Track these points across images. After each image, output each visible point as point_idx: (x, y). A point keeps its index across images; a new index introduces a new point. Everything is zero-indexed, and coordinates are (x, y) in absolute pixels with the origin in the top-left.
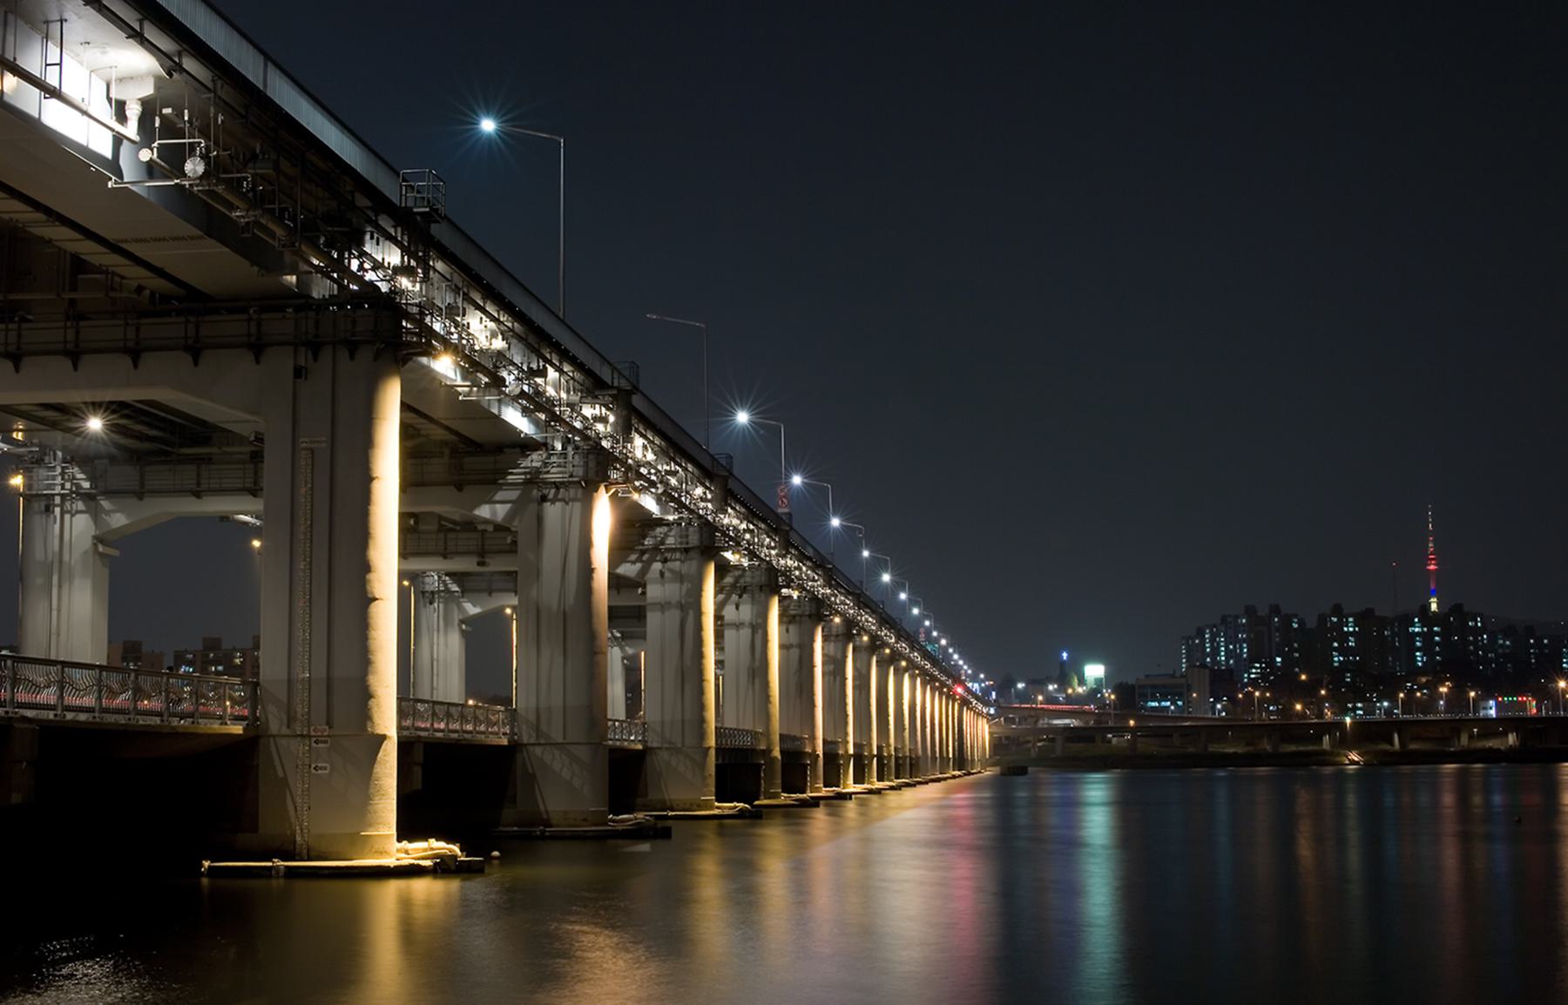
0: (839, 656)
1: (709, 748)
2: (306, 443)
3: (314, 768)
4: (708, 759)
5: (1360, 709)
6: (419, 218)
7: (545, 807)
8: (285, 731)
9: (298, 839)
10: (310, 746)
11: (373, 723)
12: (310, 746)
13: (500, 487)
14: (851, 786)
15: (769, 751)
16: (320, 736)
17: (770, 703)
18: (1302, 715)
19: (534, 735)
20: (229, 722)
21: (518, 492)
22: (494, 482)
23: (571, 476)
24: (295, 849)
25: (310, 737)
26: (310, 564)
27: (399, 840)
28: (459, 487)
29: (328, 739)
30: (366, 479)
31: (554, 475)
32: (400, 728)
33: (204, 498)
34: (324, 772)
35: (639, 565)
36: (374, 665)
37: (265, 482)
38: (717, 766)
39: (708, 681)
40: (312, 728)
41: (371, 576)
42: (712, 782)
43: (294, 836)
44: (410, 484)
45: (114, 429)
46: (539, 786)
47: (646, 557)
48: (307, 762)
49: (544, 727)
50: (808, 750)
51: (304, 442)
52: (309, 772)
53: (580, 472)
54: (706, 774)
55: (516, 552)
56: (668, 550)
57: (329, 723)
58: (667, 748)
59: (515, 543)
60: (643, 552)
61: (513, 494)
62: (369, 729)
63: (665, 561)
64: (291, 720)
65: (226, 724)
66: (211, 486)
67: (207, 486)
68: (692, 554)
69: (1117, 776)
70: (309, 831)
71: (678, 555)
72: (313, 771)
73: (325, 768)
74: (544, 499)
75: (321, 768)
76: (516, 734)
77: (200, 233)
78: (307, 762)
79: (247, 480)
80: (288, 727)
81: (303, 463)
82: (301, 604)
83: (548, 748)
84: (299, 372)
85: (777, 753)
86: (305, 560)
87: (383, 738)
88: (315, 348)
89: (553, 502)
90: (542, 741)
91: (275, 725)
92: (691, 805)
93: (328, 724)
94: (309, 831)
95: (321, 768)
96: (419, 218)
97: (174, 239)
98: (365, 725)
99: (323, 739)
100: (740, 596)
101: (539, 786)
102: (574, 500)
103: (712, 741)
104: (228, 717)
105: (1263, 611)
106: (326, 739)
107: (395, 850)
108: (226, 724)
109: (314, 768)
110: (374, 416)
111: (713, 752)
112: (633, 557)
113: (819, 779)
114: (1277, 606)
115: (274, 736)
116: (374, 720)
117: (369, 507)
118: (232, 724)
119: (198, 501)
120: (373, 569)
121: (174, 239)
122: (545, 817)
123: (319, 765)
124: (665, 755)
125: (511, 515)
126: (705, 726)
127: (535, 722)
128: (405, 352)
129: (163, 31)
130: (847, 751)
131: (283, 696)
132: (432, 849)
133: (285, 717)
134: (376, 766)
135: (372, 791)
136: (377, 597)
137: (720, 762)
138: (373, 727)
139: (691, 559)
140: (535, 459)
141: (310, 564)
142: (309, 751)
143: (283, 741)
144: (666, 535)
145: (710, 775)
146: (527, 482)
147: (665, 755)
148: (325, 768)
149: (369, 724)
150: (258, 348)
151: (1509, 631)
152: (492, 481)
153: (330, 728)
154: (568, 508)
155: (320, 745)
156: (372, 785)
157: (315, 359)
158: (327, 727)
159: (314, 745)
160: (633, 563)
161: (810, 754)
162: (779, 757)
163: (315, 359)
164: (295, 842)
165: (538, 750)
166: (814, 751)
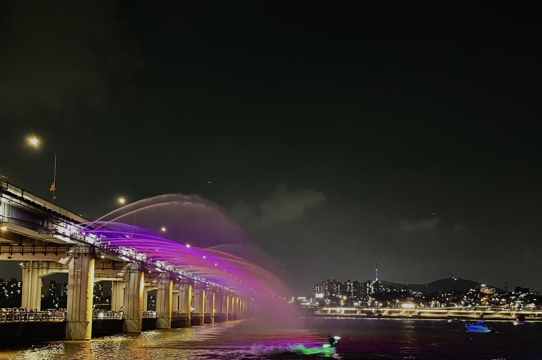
0: (212, 295)
1: (170, 318)
5: (444, 295)
13: (122, 270)
21: (126, 271)
22: (121, 269)
23: (136, 268)
28: (114, 269)
31: (133, 268)
35: (157, 281)
45: (26, 218)
47: (158, 279)
53: (138, 267)
56: (163, 278)
60: (158, 278)
61: (125, 271)
63: (162, 280)
68: (168, 279)
71: (165, 279)
74: (131, 272)
85: (190, 318)
89: (132, 273)
90: (129, 319)
100: (183, 285)
102: (137, 273)
105: (331, 281)
112: (156, 279)
114: (335, 280)
124: (160, 319)
125: (124, 275)
129: (67, 262)
130: (212, 315)
137: (172, 320)
139: (168, 280)
140: (129, 264)
144: (163, 275)
146: (127, 269)
147: (160, 319)
151: (390, 287)
152: (121, 268)
154: (135, 274)
160: (155, 280)
162: (190, 318)
165: (128, 320)
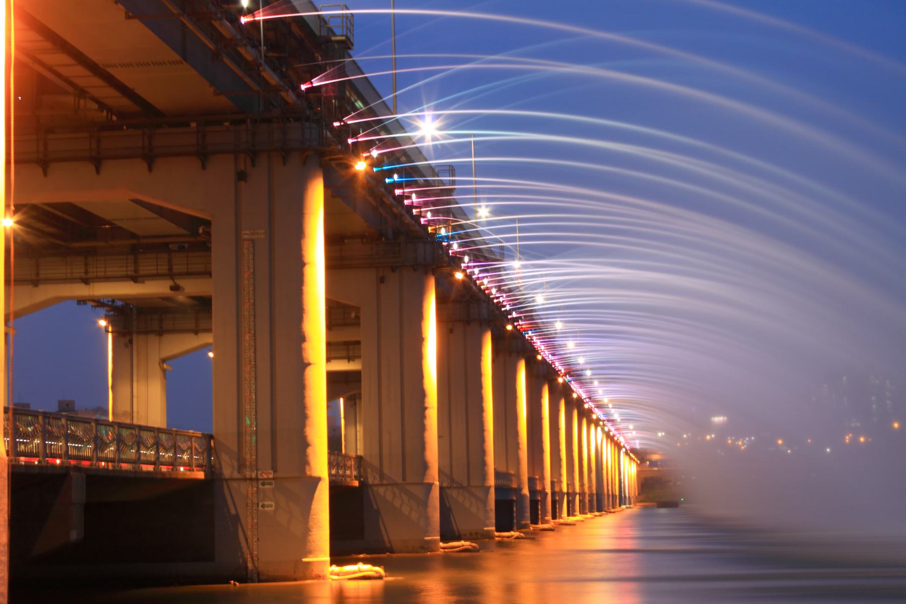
2: (248, 235)
3: (262, 506)
4: (489, 496)
6: (336, 46)
7: (388, 537)
8: (236, 475)
9: (250, 565)
10: (258, 488)
11: (311, 467)
12: (258, 488)
14: (565, 517)
15: (519, 489)
16: (266, 479)
17: (520, 449)
18: (183, 474)
19: (377, 477)
20: (195, 469)
24: (247, 574)
25: (257, 479)
26: (255, 335)
27: (332, 563)
29: (273, 482)
30: (299, 264)
32: (330, 475)
33: (91, 284)
34: (269, 509)
36: (310, 419)
37: (215, 267)
38: (497, 502)
39: (489, 431)
40: (259, 472)
41: (306, 345)
42: (492, 515)
43: (245, 562)
44: (333, 265)
46: (382, 520)
48: (255, 501)
49: (386, 471)
50: (514, 485)
51: (246, 234)
52: (257, 510)
54: (488, 508)
55: (359, 324)
57: (274, 469)
58: (455, 488)
59: (357, 318)
62: (308, 472)
64: (241, 466)
65: (193, 470)
66: (159, 272)
67: (95, 274)
69: (639, 507)
70: (258, 559)
72: (260, 508)
73: (271, 506)
75: (268, 506)
76: (362, 477)
77: (178, 57)
78: (255, 501)
79: (129, 269)
80: (239, 472)
81: (245, 251)
82: (247, 369)
83: (390, 488)
84: (241, 176)
86: (249, 333)
87: (318, 480)
88: (253, 154)
90: (385, 482)
91: (227, 471)
92: (471, 534)
93: (272, 469)
94: (258, 559)
95: (268, 506)
96: (336, 46)
97: (155, 64)
98: (304, 469)
99: (268, 481)
101: (382, 520)
103: (491, 481)
104: (194, 465)
106: (271, 481)
107: (329, 574)
108: (193, 470)
109: (262, 506)
110: (305, 212)
111: (492, 491)
113: (548, 514)
115: (227, 480)
116: (311, 465)
117: (303, 287)
118: (197, 470)
119: (87, 286)
120: (307, 339)
121: (155, 64)
122: (388, 545)
123: (266, 503)
126: (486, 468)
127: (378, 466)
128: (328, 158)
131: (234, 448)
132: (360, 571)
133: (236, 464)
134: (313, 503)
135: (311, 523)
136: (311, 362)
138: (310, 470)
141: (255, 335)
142: (257, 492)
143: (234, 485)
145: (491, 510)
148: (271, 506)
149: (307, 468)
150: (203, 155)
153: (274, 472)
155: (267, 487)
156: (311, 519)
157: (253, 165)
158: (272, 472)
159: (261, 486)
161: (540, 492)
163: (253, 165)
164: (246, 567)
165: (381, 490)
166: (544, 489)
